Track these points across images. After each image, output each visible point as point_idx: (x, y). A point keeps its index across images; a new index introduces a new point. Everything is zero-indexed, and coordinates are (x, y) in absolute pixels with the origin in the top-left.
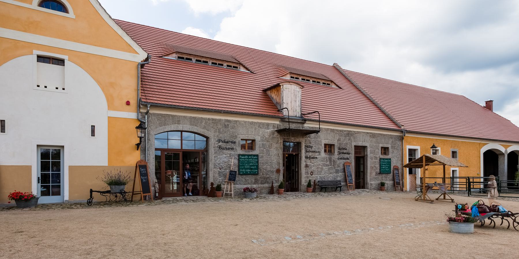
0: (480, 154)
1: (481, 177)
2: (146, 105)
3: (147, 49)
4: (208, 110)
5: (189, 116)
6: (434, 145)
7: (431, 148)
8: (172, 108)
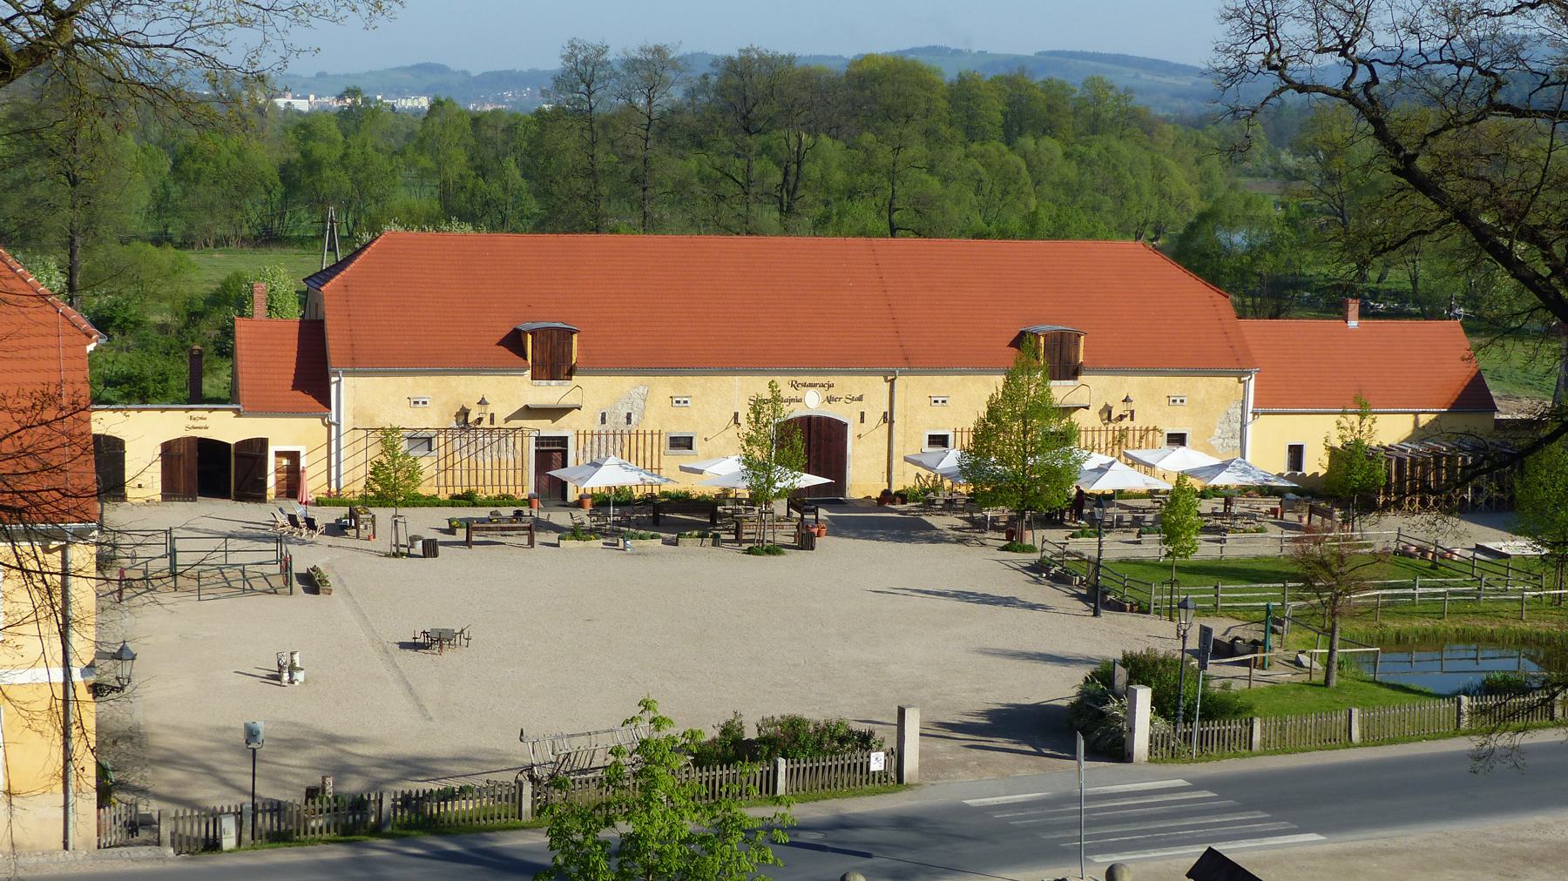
6: (483, 399)
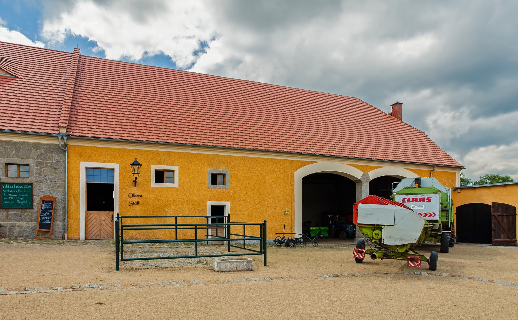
0: (292, 185)
1: (211, 229)
2: (57, 137)
3: (164, 95)
4: (219, 147)
5: (128, 148)
6: (136, 161)
7: (131, 165)
8: (84, 139)
